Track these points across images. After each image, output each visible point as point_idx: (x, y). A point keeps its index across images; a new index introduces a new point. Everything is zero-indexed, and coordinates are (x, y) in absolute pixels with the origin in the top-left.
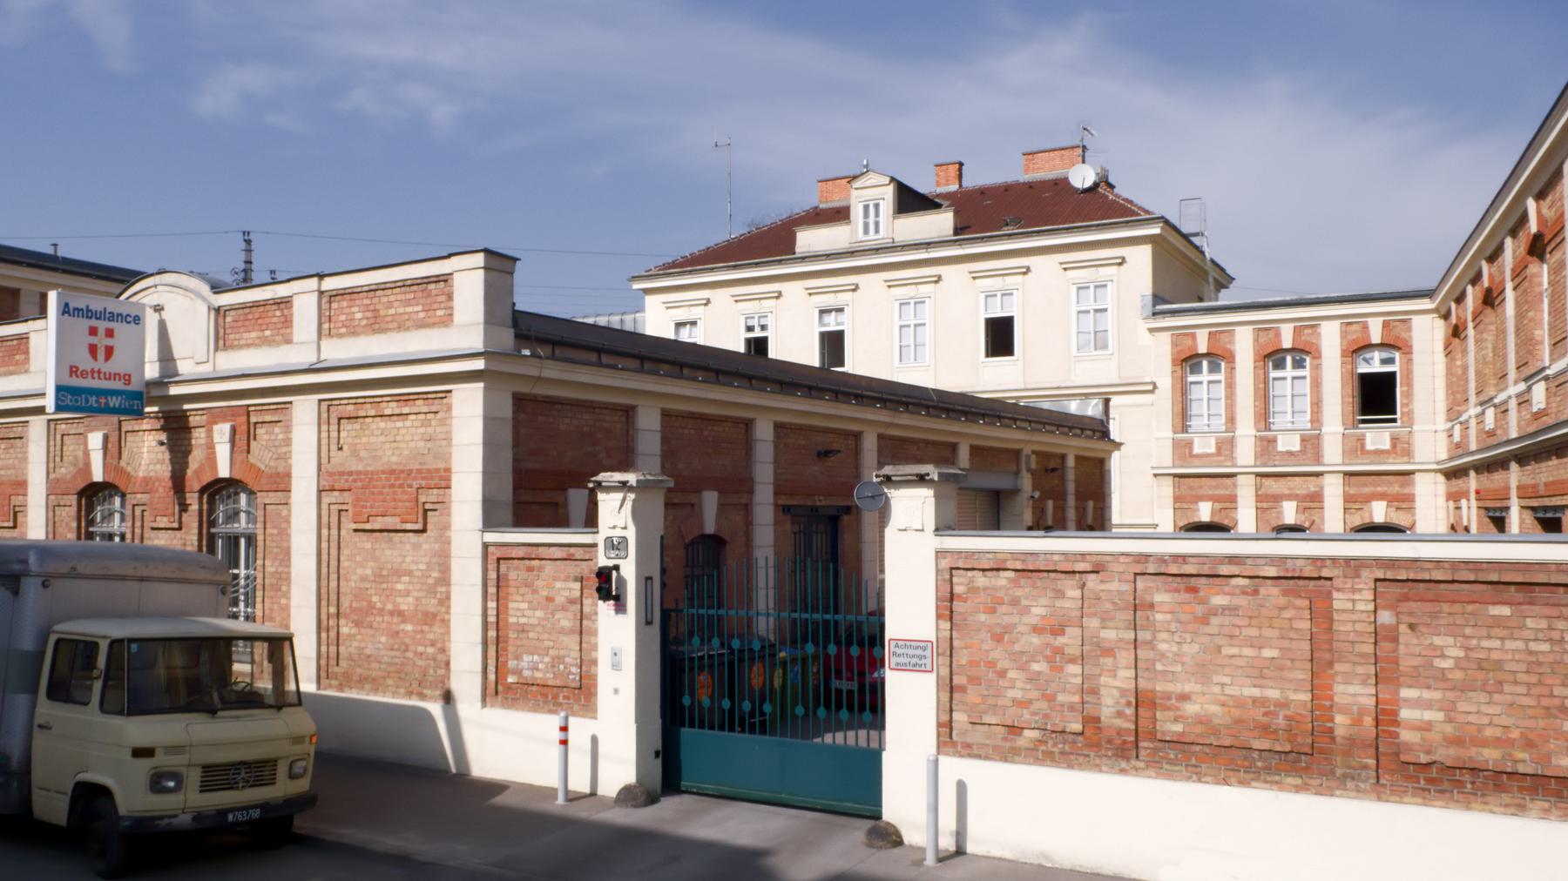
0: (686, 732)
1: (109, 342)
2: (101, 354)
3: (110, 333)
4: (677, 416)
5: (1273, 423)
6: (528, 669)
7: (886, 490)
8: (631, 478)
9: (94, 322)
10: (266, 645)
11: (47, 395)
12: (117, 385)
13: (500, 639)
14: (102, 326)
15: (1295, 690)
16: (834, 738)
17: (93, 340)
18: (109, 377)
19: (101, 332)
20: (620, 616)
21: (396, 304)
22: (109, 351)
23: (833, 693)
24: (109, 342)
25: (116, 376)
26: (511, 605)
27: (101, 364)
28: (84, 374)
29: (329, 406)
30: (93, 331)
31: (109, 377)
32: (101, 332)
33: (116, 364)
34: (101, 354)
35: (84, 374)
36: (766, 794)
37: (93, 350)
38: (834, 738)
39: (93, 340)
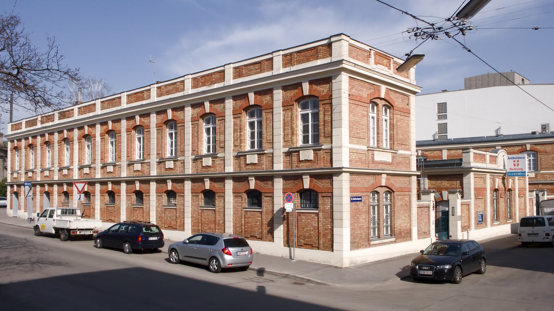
0: (416, 177)
3: (518, 161)
4: (429, 218)
9: (514, 160)
10: (285, 204)
11: (416, 206)
13: (377, 176)
14: (516, 160)
16: (468, 235)
17: (514, 163)
18: (518, 169)
19: (516, 161)
22: (518, 165)
24: (518, 163)
25: (520, 169)
27: (516, 167)
28: (513, 169)
29: (330, 196)
30: (514, 161)
31: (518, 169)
32: (516, 161)
33: (519, 167)
34: (516, 165)
35: (513, 169)
37: (514, 165)
38: (468, 235)
39: (514, 163)
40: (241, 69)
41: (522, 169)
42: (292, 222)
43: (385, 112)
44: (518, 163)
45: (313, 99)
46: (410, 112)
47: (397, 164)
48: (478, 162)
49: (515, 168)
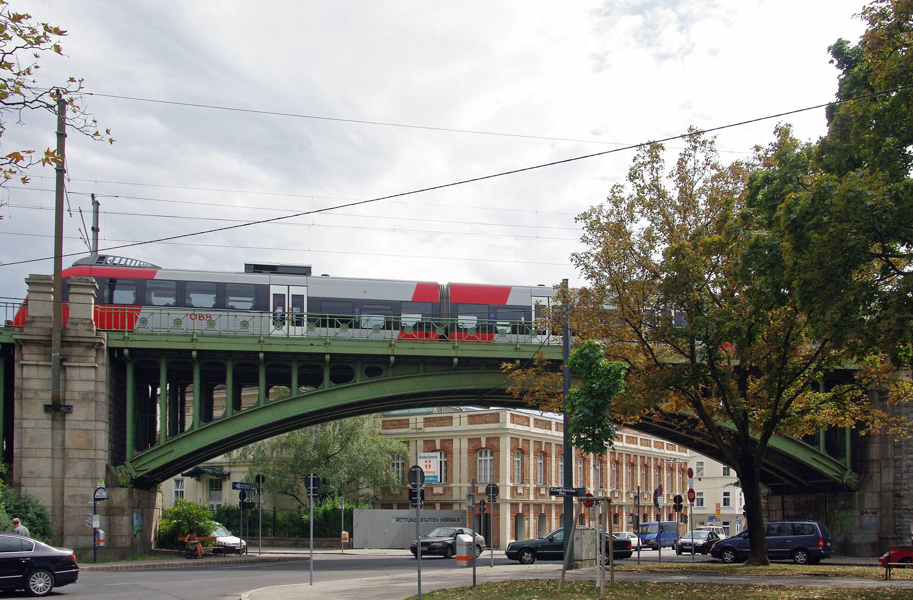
1: (430, 464)
2: (428, 467)
3: (430, 461)
5: (771, 144)
6: (607, 356)
7: (760, 485)
8: (641, 543)
12: (432, 475)
14: (428, 460)
15: (433, 592)
17: (426, 464)
19: (428, 461)
20: (833, 42)
21: (296, 310)
22: (430, 466)
23: (467, 525)
24: (430, 464)
26: (187, 399)
30: (426, 462)
32: (428, 461)
34: (428, 467)
36: (391, 394)
39: (426, 464)
41: (434, 472)
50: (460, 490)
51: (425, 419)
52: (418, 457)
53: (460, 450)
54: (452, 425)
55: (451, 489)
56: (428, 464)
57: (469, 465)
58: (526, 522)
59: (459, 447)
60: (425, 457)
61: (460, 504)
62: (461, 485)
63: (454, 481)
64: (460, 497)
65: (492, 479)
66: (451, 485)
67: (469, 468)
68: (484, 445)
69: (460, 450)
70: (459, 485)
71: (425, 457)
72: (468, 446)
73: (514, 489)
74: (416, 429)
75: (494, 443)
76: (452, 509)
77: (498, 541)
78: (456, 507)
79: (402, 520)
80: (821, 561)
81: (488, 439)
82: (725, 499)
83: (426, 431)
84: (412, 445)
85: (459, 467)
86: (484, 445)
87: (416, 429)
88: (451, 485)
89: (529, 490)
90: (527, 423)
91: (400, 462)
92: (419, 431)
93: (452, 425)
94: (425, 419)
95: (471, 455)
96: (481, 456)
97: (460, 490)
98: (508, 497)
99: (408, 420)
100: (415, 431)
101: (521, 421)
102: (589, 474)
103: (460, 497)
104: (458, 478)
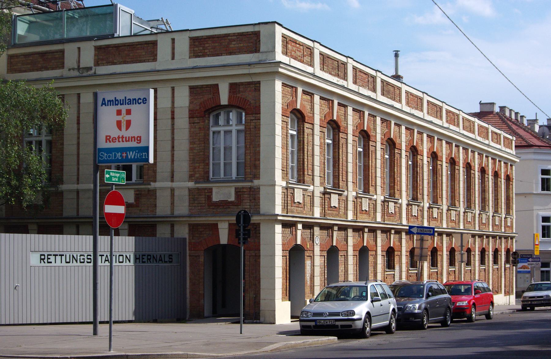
3: (129, 112)
9: (119, 107)
14: (124, 108)
17: (119, 118)
19: (124, 112)
22: (129, 123)
24: (128, 117)
25: (132, 138)
28: (114, 140)
30: (119, 113)
32: (124, 112)
33: (132, 132)
35: (114, 140)
37: (119, 124)
39: (119, 118)
40: (201, 140)
41: (139, 139)
42: (392, 220)
43: (362, 234)
44: (128, 117)
45: (216, 113)
46: (423, 155)
47: (256, 277)
48: (485, 262)
49: (121, 134)
50: (173, 195)
51: (98, 49)
52: (100, 102)
53: (173, 113)
54: (155, 60)
55: (152, 193)
56: (124, 118)
57: (191, 143)
58: (308, 263)
59: (170, 105)
60: (116, 102)
61: (172, 226)
62: (175, 185)
63: (159, 177)
64: (172, 209)
65: (242, 171)
66: (153, 185)
67: (191, 149)
68: (224, 100)
69: (173, 113)
70: (169, 184)
71: (116, 102)
72: (191, 103)
73: (288, 191)
74: (79, 68)
75: (249, 96)
76: (154, 235)
77: (257, 302)
78: (163, 231)
79: (52, 259)
80: (411, 296)
81: (233, 87)
82: (543, 227)
83: (98, 72)
84: (72, 101)
85: (169, 147)
86: (224, 100)
87: (79, 68)
88: (153, 185)
89: (312, 197)
90: (307, 59)
91: (44, 138)
92: (85, 74)
93: (155, 60)
94: (98, 49)
95: (196, 120)
96: (216, 123)
97: (173, 195)
98: (278, 210)
99: (62, 52)
100: (76, 73)
101: (298, 54)
102: (401, 174)
103: (172, 209)
104: (169, 169)
